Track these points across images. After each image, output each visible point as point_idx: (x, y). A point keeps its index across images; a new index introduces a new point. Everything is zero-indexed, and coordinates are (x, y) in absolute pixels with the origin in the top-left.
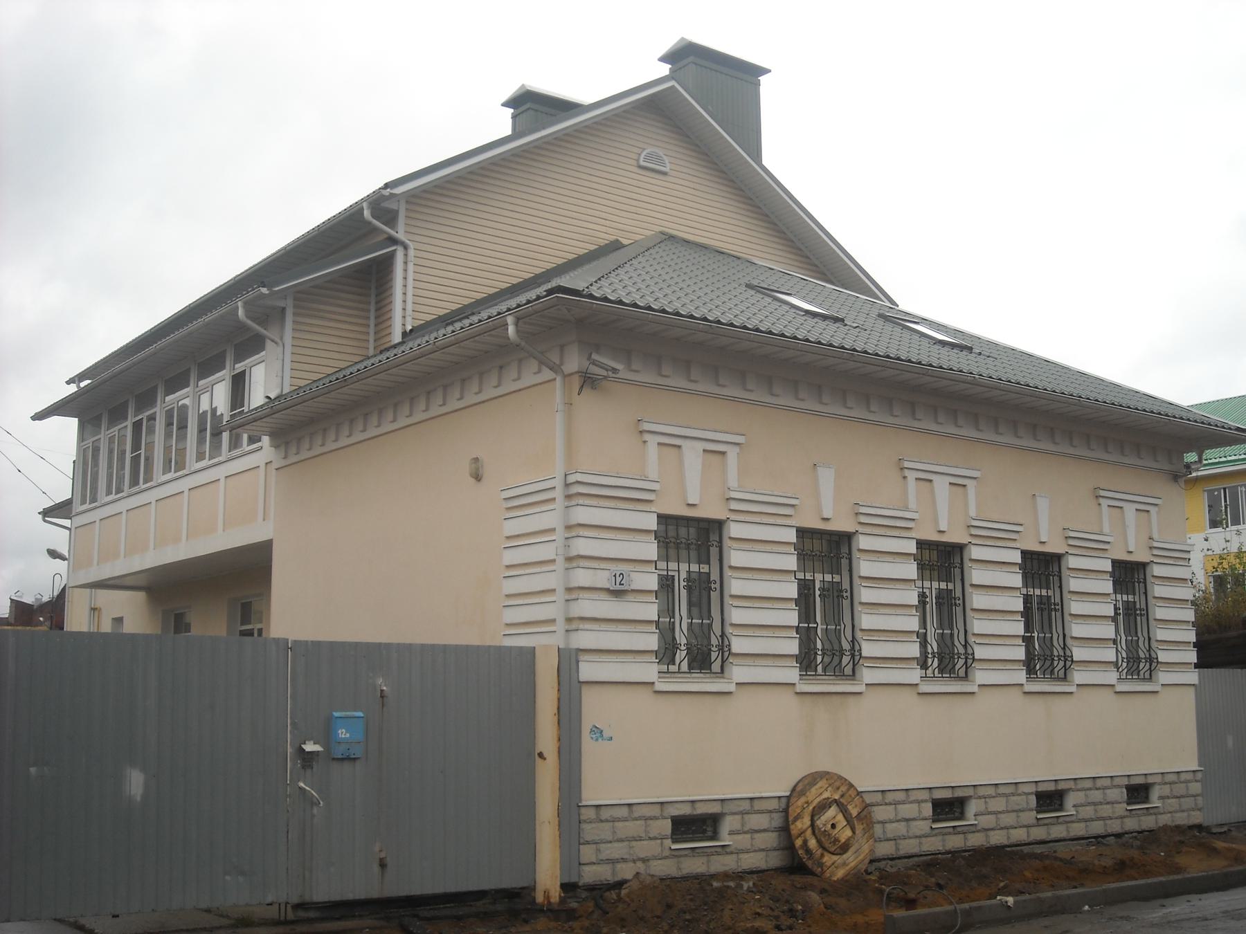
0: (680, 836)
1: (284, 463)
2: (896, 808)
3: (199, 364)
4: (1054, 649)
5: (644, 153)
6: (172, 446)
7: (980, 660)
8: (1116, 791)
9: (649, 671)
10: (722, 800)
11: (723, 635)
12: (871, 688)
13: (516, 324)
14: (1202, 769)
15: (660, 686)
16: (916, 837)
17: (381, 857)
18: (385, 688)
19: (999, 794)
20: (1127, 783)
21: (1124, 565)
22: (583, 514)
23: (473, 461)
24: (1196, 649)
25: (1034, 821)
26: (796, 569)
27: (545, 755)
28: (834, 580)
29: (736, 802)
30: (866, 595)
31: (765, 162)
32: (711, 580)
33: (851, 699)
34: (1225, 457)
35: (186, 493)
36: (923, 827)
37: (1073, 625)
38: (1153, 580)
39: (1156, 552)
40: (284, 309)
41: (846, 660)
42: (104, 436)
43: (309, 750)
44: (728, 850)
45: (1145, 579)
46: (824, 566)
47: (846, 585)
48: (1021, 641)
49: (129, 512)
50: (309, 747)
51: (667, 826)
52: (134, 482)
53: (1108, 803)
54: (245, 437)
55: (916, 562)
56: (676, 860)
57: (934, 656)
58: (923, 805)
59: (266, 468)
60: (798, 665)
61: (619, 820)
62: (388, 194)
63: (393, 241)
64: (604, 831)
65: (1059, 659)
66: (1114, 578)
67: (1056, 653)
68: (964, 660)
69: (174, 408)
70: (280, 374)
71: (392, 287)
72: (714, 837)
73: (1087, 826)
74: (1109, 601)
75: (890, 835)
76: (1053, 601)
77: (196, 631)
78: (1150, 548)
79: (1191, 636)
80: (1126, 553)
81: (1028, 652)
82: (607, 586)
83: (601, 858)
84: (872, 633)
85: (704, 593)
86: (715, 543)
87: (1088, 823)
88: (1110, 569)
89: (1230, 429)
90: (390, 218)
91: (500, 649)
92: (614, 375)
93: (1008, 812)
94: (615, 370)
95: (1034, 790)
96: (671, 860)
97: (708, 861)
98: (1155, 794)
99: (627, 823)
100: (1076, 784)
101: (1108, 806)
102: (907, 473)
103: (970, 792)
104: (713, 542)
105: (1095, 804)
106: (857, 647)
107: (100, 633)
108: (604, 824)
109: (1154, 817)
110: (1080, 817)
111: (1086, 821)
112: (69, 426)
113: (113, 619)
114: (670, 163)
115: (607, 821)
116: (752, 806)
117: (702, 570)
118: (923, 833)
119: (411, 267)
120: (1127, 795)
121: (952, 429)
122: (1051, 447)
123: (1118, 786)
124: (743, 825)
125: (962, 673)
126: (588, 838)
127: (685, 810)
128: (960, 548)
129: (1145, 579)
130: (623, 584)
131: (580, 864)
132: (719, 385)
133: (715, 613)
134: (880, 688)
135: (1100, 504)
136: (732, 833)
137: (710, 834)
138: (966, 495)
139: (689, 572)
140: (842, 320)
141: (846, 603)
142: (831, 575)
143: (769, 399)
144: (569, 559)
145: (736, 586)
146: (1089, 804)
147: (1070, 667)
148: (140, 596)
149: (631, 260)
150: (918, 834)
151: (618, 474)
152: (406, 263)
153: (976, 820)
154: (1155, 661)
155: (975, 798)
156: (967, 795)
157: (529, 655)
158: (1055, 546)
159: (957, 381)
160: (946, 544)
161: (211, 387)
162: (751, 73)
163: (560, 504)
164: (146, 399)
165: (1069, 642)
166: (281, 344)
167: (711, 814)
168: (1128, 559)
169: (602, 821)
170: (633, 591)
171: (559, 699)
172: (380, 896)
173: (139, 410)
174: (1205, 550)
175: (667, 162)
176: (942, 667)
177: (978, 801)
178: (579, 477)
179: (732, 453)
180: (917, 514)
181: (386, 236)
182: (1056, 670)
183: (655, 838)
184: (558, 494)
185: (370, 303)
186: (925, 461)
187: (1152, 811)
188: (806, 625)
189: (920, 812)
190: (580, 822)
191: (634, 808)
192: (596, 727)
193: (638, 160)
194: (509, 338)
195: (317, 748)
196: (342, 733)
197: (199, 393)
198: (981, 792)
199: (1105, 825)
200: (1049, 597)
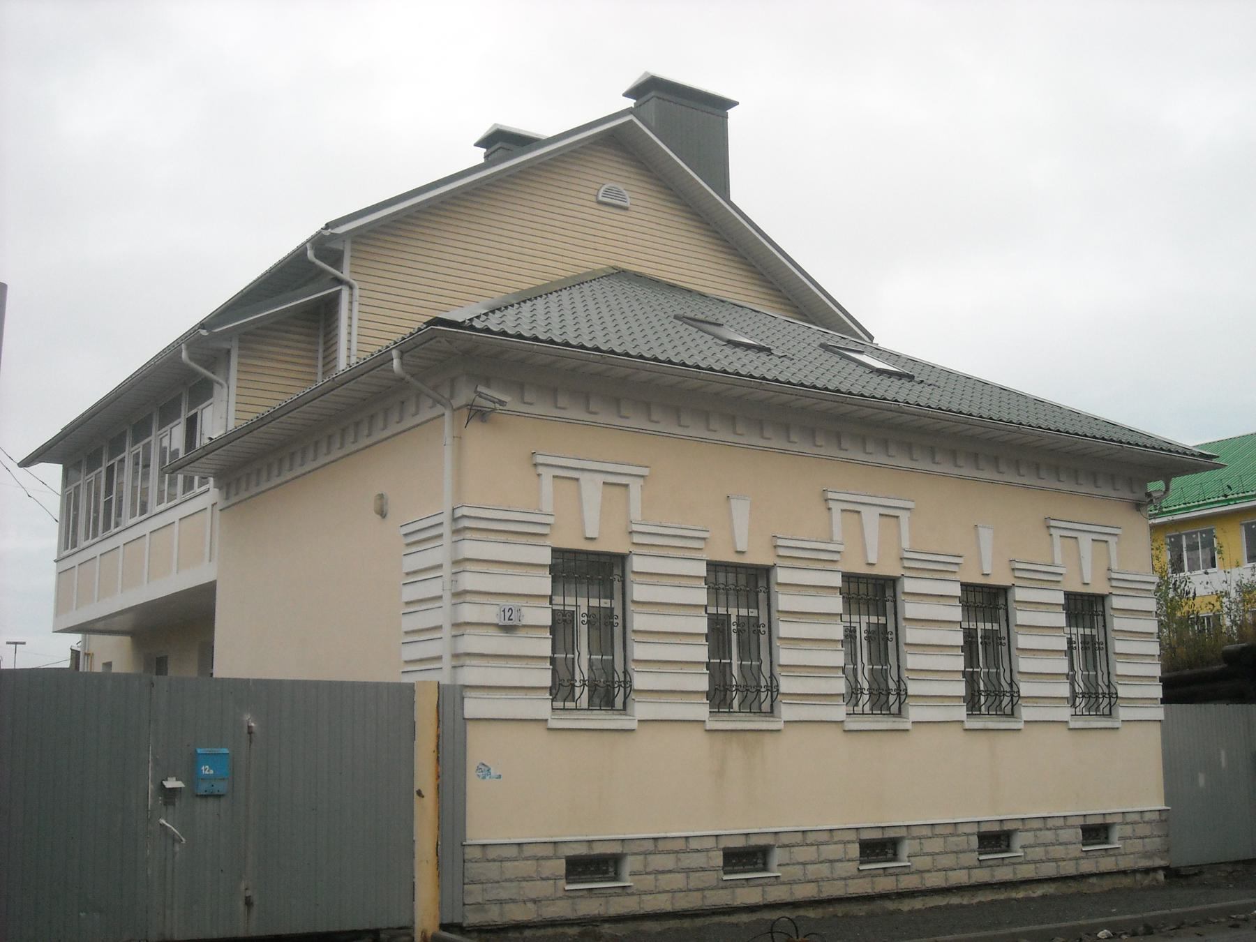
0: (577, 877)
1: (226, 505)
2: (818, 849)
3: (161, 408)
4: (616, 674)
5: (603, 189)
6: (164, 490)
7: (783, 694)
8: (1071, 832)
9: (542, 707)
10: (623, 840)
11: (772, 676)
12: (1029, 725)
13: (401, 358)
14: (1169, 808)
15: (553, 724)
16: (841, 879)
17: (247, 895)
18: (253, 724)
19: (936, 835)
20: (1083, 823)
21: (874, 581)
22: (470, 549)
23: (378, 497)
24: (1161, 684)
25: (977, 863)
26: (841, 612)
27: (423, 793)
28: (880, 622)
29: (638, 842)
30: (785, 629)
31: (732, 199)
32: (888, 631)
33: (768, 737)
34: (1238, 494)
35: (148, 536)
36: (851, 868)
37: (1020, 659)
38: (1112, 612)
39: (1115, 583)
40: (228, 352)
41: (892, 698)
42: (83, 480)
43: (170, 787)
44: (629, 891)
45: (1104, 611)
46: (870, 609)
47: (891, 628)
48: (961, 677)
49: (102, 556)
50: (171, 783)
51: (561, 867)
52: (107, 527)
53: (1061, 844)
54: (196, 478)
55: (841, 596)
56: (570, 901)
57: (584, 685)
58: (849, 846)
59: (212, 510)
60: (708, 702)
61: (508, 859)
62: (328, 234)
63: (340, 281)
64: (492, 870)
65: (1104, 697)
66: (1068, 611)
67: (1100, 691)
68: (1010, 698)
69: (139, 452)
70: (224, 416)
71: (337, 327)
72: (616, 878)
73: (1036, 868)
74: (1062, 634)
75: (810, 877)
76: (1097, 640)
77: (173, 671)
78: (1013, 569)
79: (1157, 671)
80: (1080, 584)
81: (1073, 691)
82: (496, 621)
83: (487, 898)
84: (793, 669)
85: (753, 637)
86: (890, 598)
87: (1038, 865)
88: (1062, 601)
89: (1193, 455)
90: (336, 259)
91: (400, 684)
92: (501, 408)
93: (946, 853)
94: (502, 403)
95: (976, 830)
96: (566, 901)
97: (607, 903)
98: (1116, 834)
99: (516, 863)
100: (1024, 824)
101: (1061, 847)
102: (831, 504)
103: (902, 833)
104: (615, 577)
105: (1045, 845)
106: (903, 687)
107: (93, 673)
108: (491, 864)
109: (1113, 858)
110: (1029, 858)
111: (1035, 862)
112: (53, 472)
113: (104, 664)
114: (630, 197)
115: (494, 860)
116: (656, 846)
117: (750, 615)
118: (849, 874)
119: (356, 306)
120: (1083, 835)
121: (883, 459)
122: (1113, 494)
123: (1073, 827)
124: (645, 866)
125: (1008, 710)
126: (717, 574)
127: (582, 850)
128: (893, 582)
129: (1104, 611)
130: (512, 620)
131: (464, 904)
132: (621, 417)
133: (764, 655)
134: (513, 724)
135: (1051, 535)
136: (633, 874)
137: (612, 874)
138: (899, 526)
139: (869, 623)
140: (769, 350)
141: (891, 645)
142: (876, 617)
143: (678, 431)
144: (457, 594)
145: (639, 621)
146: (1039, 845)
147: (904, 701)
148: (127, 640)
149: (561, 290)
150: (700, 887)
151: (509, 507)
152: (351, 303)
153: (909, 861)
154: (1114, 696)
155: (908, 839)
156: (899, 835)
157: (405, 694)
158: (1000, 578)
159: (941, 419)
160: (877, 578)
161: (169, 430)
162: (719, 106)
163: (448, 538)
164: (117, 447)
165: (1017, 677)
166: (225, 385)
167: (762, 846)
168: (1084, 591)
169: (488, 861)
170: (524, 626)
171: (438, 736)
172: (246, 935)
173: (112, 457)
174: (1205, 583)
175: (627, 196)
176: (1089, 705)
177: (913, 842)
178: (465, 511)
179: (635, 486)
180: (843, 546)
181: (332, 277)
182: (1101, 707)
183: (548, 879)
184: (446, 530)
185: (318, 343)
186: (853, 492)
187: (1111, 852)
188: (971, 670)
189: (846, 853)
190: (464, 862)
191: (525, 847)
192: (483, 764)
193: (597, 196)
194: (393, 372)
195: (179, 784)
196: (205, 769)
197: (161, 436)
198: (915, 832)
199: (1058, 866)
200: (1093, 636)
